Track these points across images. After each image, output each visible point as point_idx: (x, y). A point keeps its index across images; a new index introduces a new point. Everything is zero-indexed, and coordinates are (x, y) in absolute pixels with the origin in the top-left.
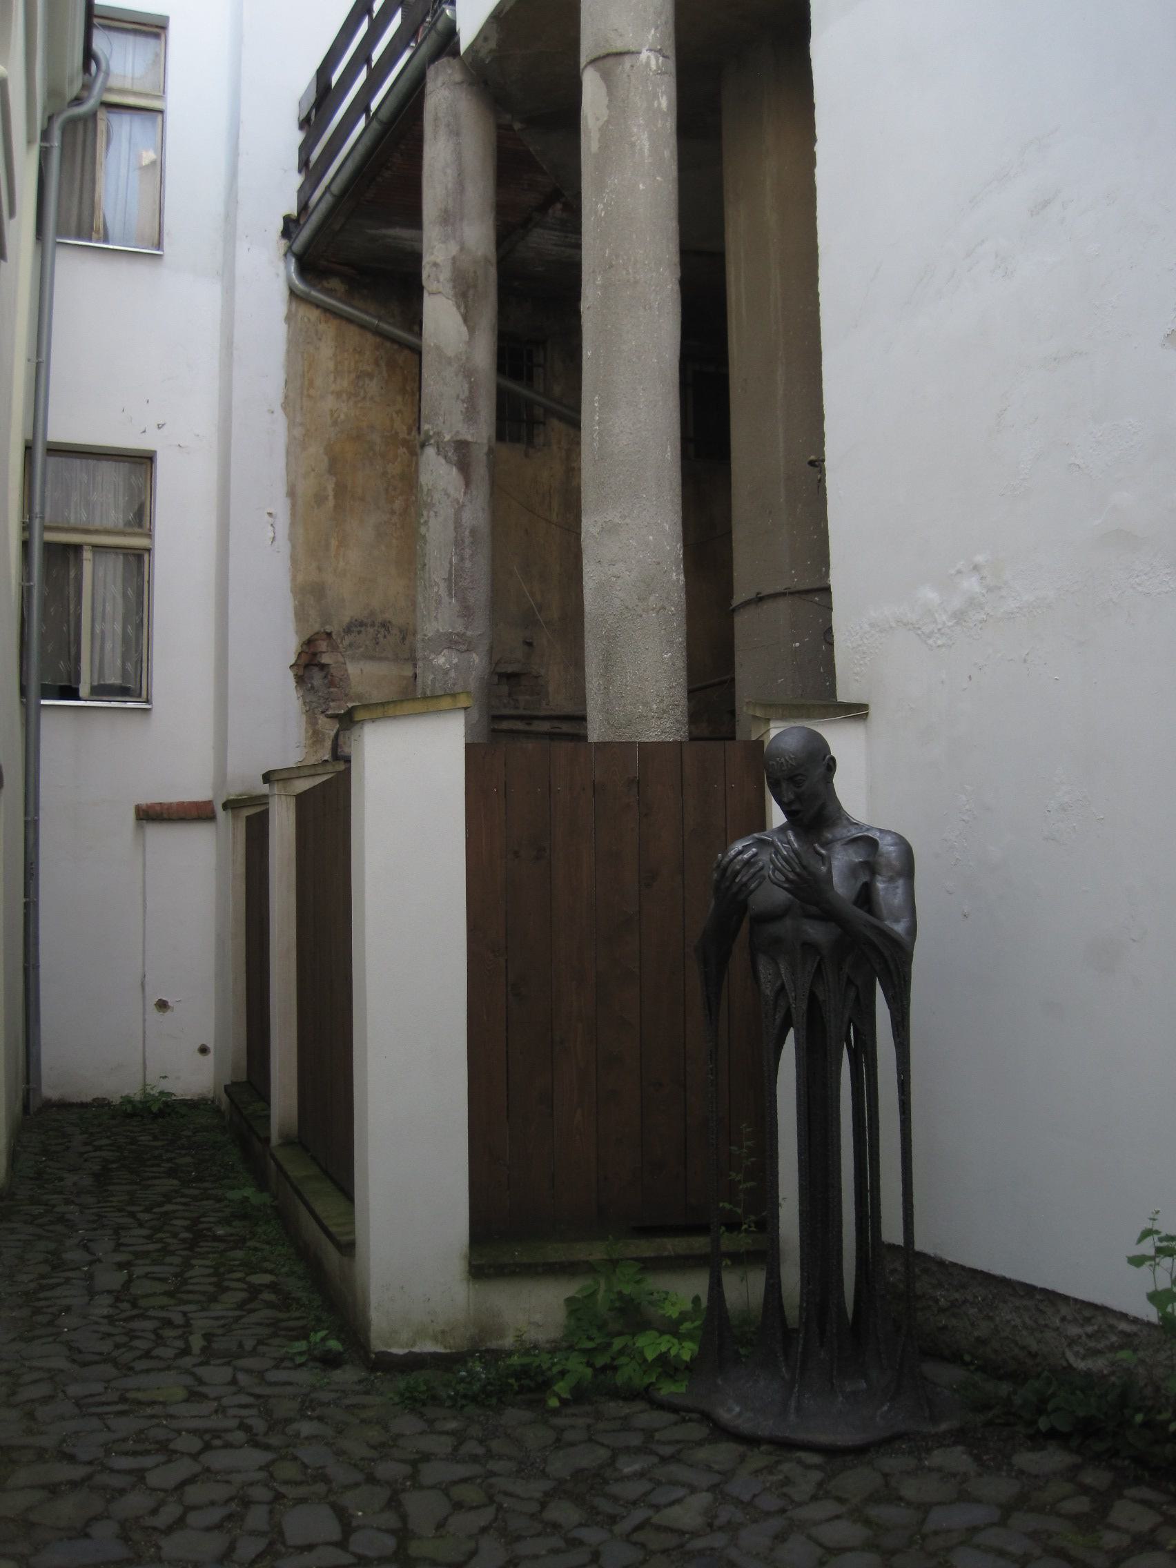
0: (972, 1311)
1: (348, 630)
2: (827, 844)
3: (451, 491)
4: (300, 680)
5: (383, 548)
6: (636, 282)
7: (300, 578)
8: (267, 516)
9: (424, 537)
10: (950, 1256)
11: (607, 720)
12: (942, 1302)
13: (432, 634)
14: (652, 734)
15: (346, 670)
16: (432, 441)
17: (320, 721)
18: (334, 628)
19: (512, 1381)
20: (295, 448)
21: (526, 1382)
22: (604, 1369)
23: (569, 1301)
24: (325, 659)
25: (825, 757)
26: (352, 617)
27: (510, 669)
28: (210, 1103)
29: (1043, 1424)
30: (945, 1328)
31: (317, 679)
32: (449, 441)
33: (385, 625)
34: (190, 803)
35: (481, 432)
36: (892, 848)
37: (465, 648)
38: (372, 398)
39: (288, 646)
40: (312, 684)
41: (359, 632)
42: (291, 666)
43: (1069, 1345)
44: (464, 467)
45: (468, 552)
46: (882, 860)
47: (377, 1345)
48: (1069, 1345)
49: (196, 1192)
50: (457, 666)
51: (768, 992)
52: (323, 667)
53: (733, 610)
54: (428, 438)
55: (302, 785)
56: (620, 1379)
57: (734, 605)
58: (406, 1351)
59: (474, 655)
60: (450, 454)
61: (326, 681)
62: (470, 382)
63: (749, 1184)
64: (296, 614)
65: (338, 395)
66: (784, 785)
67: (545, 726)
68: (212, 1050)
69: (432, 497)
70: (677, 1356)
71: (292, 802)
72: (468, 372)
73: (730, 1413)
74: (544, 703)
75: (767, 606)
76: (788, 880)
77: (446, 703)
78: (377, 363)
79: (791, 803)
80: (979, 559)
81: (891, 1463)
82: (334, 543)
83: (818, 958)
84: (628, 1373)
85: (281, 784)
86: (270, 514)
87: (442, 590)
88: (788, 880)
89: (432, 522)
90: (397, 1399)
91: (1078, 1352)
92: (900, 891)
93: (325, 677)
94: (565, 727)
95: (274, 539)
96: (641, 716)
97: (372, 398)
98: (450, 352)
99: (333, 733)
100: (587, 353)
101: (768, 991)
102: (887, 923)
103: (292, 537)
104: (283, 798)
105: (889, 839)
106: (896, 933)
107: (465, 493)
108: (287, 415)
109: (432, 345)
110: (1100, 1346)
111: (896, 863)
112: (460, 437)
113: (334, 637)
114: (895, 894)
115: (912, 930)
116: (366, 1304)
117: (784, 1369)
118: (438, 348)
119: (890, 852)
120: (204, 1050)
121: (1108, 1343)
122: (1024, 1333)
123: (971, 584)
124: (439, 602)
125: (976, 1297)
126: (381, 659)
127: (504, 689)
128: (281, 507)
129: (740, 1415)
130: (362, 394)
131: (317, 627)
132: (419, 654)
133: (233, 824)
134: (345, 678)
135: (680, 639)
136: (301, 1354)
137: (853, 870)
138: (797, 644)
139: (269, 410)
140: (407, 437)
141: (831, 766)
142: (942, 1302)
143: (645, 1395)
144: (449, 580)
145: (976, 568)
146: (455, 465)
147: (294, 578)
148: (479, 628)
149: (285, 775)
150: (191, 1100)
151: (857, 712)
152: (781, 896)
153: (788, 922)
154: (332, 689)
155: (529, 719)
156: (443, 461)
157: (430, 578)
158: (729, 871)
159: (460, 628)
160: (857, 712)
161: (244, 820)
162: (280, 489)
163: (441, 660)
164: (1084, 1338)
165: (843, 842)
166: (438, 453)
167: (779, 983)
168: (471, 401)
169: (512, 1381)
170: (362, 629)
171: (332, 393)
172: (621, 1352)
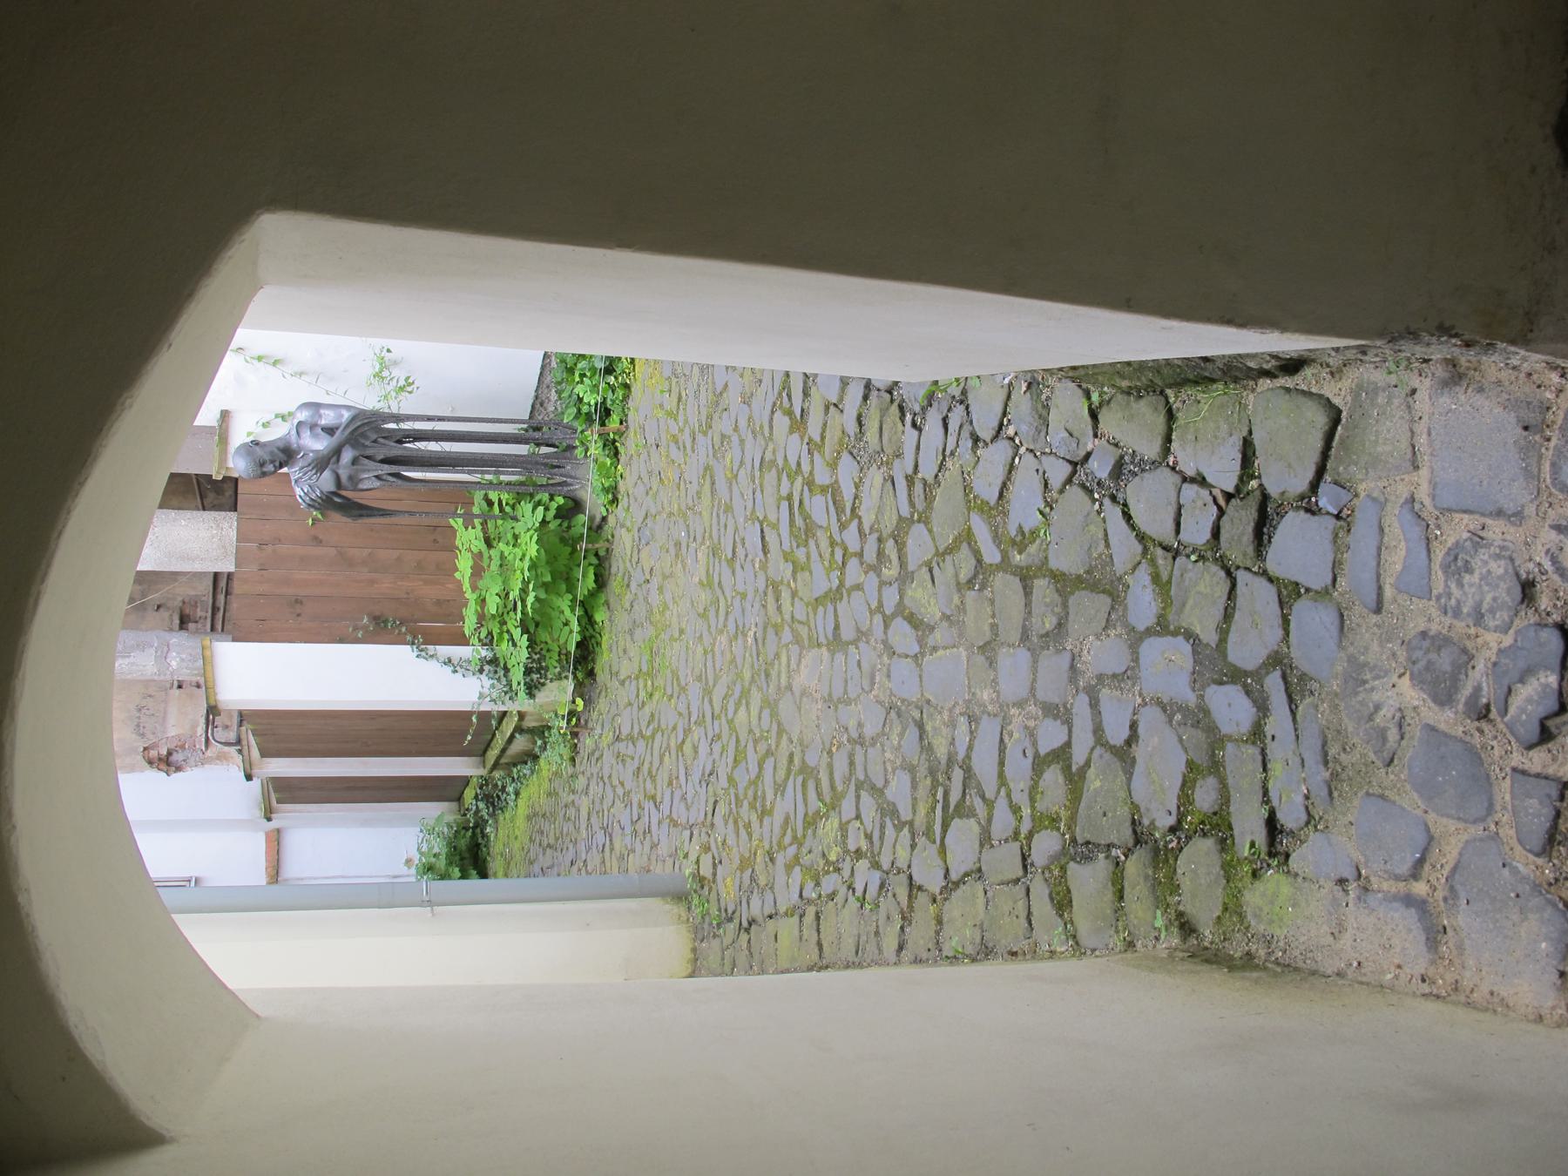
4: (179, 769)
18: (141, 746)
27: (177, 622)
31: (176, 757)
42: (168, 775)
46: (310, 420)
50: (178, 653)
52: (170, 753)
55: (255, 753)
66: (265, 469)
67: (221, 598)
74: (203, 598)
76: (316, 474)
77: (208, 653)
88: (316, 474)
92: (327, 412)
94: (222, 584)
101: (377, 483)
115: (348, 408)
124: (133, 664)
126: (165, 713)
127: (191, 626)
131: (140, 757)
137: (315, 436)
148: (154, 638)
155: (215, 609)
159: (152, 651)
163: (174, 663)
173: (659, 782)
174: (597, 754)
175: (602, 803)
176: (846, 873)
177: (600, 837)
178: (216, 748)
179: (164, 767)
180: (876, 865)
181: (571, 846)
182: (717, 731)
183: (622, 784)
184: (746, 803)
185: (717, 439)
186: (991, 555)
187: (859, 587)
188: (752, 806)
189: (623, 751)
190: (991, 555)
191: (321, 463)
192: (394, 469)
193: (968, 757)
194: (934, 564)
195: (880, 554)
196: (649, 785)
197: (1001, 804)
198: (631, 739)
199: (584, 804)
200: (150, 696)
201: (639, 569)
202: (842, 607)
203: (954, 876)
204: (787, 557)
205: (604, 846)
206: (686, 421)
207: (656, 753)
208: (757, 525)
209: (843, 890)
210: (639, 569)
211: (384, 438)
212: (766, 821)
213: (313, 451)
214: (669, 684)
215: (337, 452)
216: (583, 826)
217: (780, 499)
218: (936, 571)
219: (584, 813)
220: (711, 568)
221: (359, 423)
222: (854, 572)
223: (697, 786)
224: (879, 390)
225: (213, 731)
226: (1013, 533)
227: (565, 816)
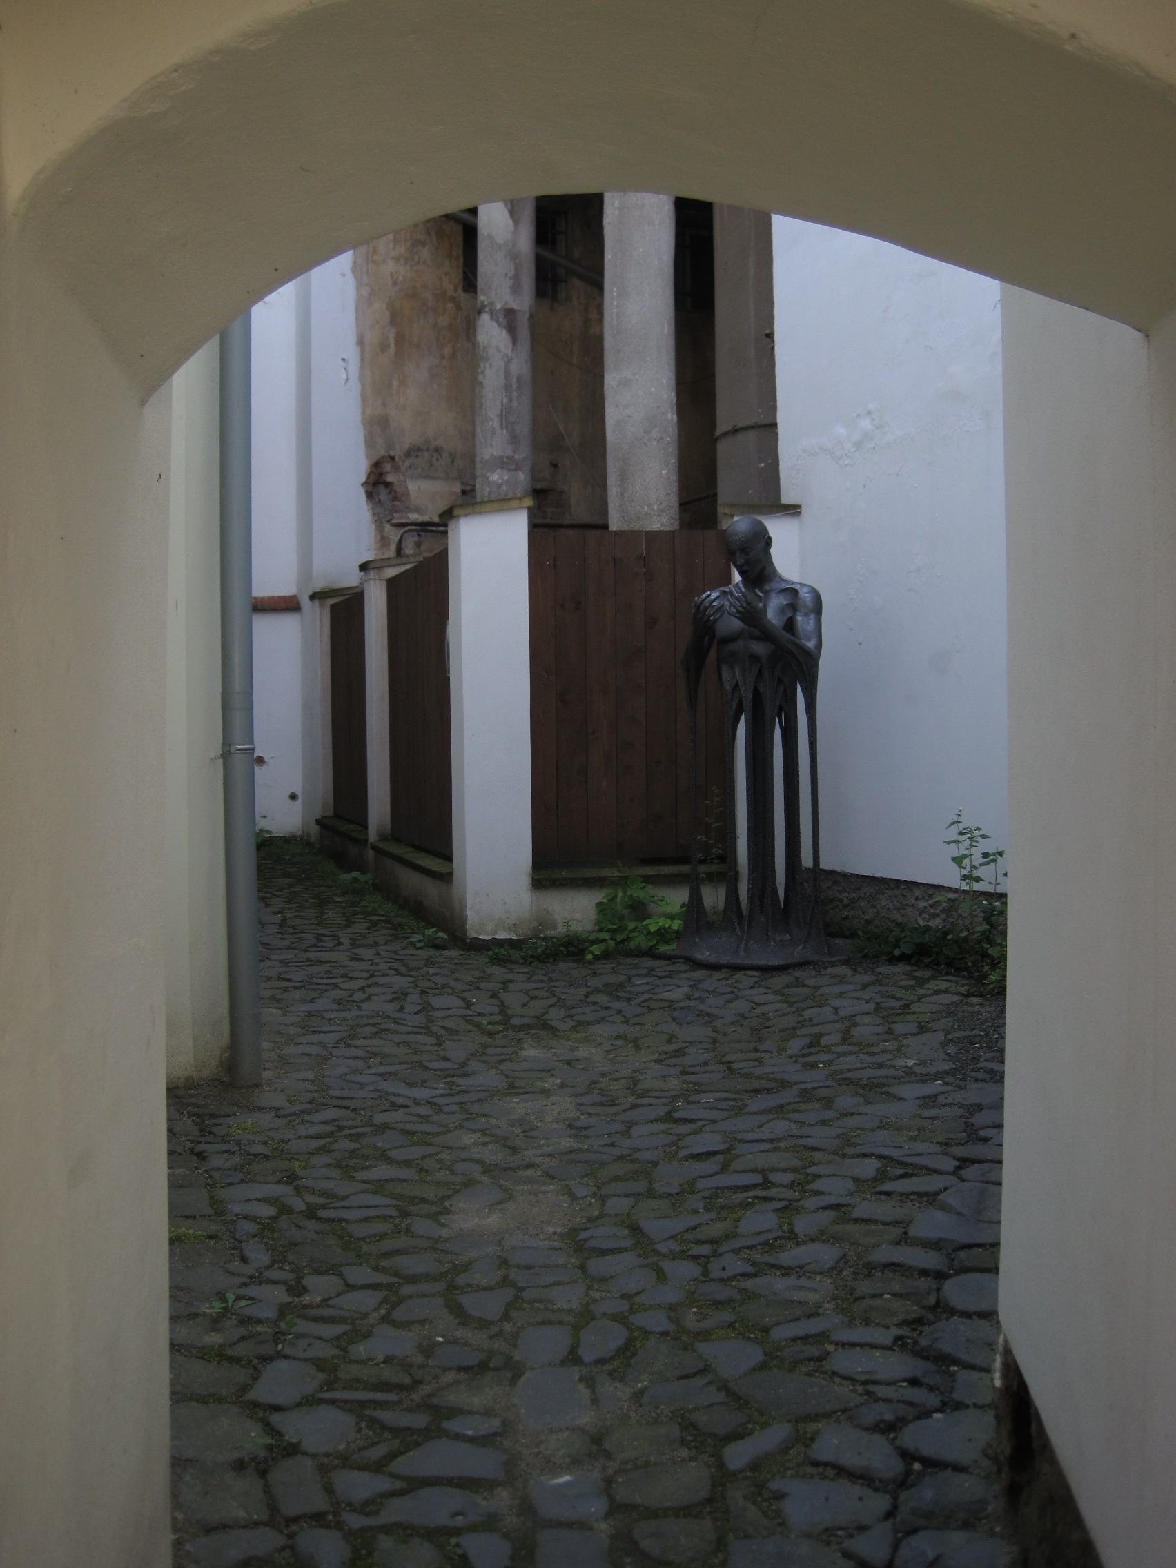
0: (863, 904)
1: (408, 454)
2: (766, 593)
3: (502, 348)
4: (370, 495)
5: (435, 386)
6: (643, 205)
7: (369, 411)
8: (341, 362)
9: (481, 383)
10: (850, 870)
11: (623, 517)
12: (846, 901)
13: (488, 457)
14: (655, 526)
15: (407, 487)
16: (487, 309)
17: (386, 529)
18: (396, 453)
19: (562, 948)
20: (363, 304)
21: (571, 949)
22: (622, 941)
23: (598, 904)
24: (390, 478)
25: (764, 536)
26: (411, 444)
27: (539, 487)
28: (299, 839)
29: (897, 952)
30: (847, 917)
31: (383, 494)
32: (500, 309)
33: (438, 450)
34: (279, 597)
35: (524, 302)
36: (807, 595)
37: (513, 467)
38: (424, 262)
39: (359, 468)
40: (379, 499)
41: (417, 456)
42: (362, 485)
43: (920, 915)
44: (511, 329)
45: (515, 394)
47: (472, 934)
48: (920, 915)
49: (309, 884)
50: (508, 481)
51: (728, 688)
52: (388, 485)
53: (716, 439)
54: (483, 306)
55: (391, 572)
56: (633, 945)
57: (716, 436)
58: (490, 937)
59: (520, 473)
60: (501, 319)
61: (390, 496)
62: (515, 264)
63: (718, 824)
64: (366, 442)
65: (397, 259)
68: (300, 798)
69: (487, 352)
70: (670, 928)
71: (384, 586)
72: (514, 256)
73: (703, 955)
75: (741, 437)
77: (515, 503)
78: (428, 233)
79: (742, 565)
80: (871, 407)
81: (798, 973)
82: (395, 383)
83: (759, 665)
84: (640, 941)
85: (376, 571)
86: (343, 360)
87: (496, 425)
89: (488, 372)
90: (487, 960)
91: (925, 918)
93: (390, 493)
95: (347, 380)
96: (646, 514)
97: (424, 262)
98: (500, 239)
99: (397, 539)
100: (608, 256)
101: (728, 687)
102: (803, 641)
103: (362, 378)
104: (377, 581)
105: (805, 589)
106: (809, 648)
107: (513, 350)
108: (356, 277)
109: (486, 234)
110: (937, 911)
111: (810, 604)
112: (509, 306)
113: (397, 459)
114: (809, 624)
115: (819, 646)
116: (463, 907)
117: (738, 930)
118: (490, 236)
119: (805, 597)
120: (293, 797)
121: (941, 908)
122: (894, 912)
123: (866, 424)
124: (493, 433)
125: (865, 894)
128: (352, 353)
129: (710, 955)
130: (416, 259)
131: (382, 452)
132: (478, 472)
133: (320, 612)
134: (406, 494)
135: (673, 460)
136: (420, 941)
137: (782, 610)
138: (763, 465)
139: (340, 274)
140: (454, 295)
141: (769, 542)
142: (846, 901)
143: (651, 954)
144: (501, 416)
145: (869, 413)
146: (504, 327)
147: (363, 413)
149: (378, 564)
150: (284, 837)
151: (793, 510)
152: (736, 625)
153: (741, 643)
154: (395, 503)
156: (495, 325)
157: (486, 414)
158: (702, 607)
159: (509, 453)
160: (793, 510)
161: (329, 610)
162: (352, 338)
164: (928, 907)
165: (777, 591)
166: (492, 318)
167: (734, 682)
168: (516, 278)
169: (562, 948)
170: (419, 454)
171: (392, 258)
172: (634, 930)
173: (376, 1042)
174: (403, 969)
175: (342, 976)
176: (274, 1274)
177: (298, 976)
178: (394, 535)
179: (373, 478)
180: (283, 1310)
181: (286, 943)
182: (446, 1109)
183: (368, 999)
184: (356, 1146)
185: (824, 1092)
186: (738, 1455)
187: (661, 1276)
188: (352, 1153)
189: (409, 999)
190: (738, 1455)
191: (752, 616)
192: (747, 704)
193: (446, 1434)
194: (710, 1377)
195: (718, 1304)
196: (369, 1030)
197: (382, 1484)
198: (426, 1008)
199: (341, 956)
200: (453, 462)
201: (640, 1010)
202: (629, 1258)
203: (276, 1418)
204: (690, 1186)
205: (289, 980)
206: (840, 1055)
207: (412, 1038)
208: (723, 1147)
209: (249, 1270)
210: (640, 1010)
211: (785, 690)
212: (334, 1173)
213: (765, 606)
214: (498, 1050)
215: (766, 635)
216: (312, 955)
217: (762, 1172)
218: (701, 1381)
219: (325, 956)
220: (656, 1094)
221: (801, 660)
222: (685, 1271)
223: (370, 1088)
224: (938, 1290)
225: (415, 530)
226: (774, 1485)
227: (324, 935)
